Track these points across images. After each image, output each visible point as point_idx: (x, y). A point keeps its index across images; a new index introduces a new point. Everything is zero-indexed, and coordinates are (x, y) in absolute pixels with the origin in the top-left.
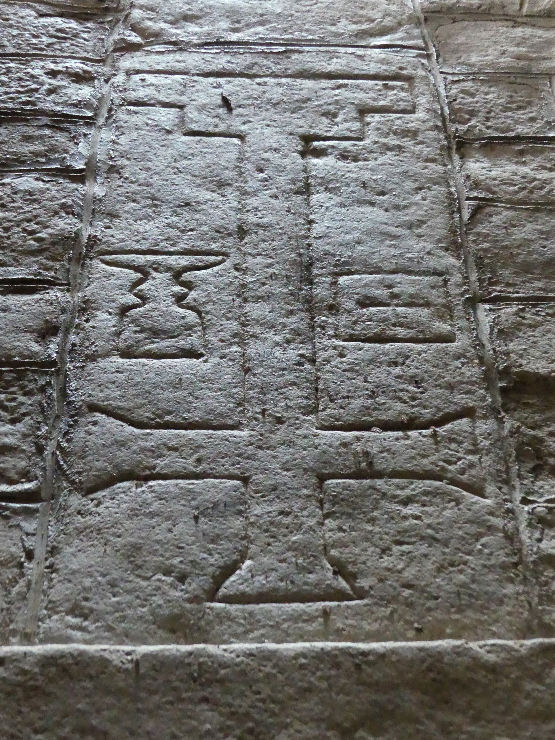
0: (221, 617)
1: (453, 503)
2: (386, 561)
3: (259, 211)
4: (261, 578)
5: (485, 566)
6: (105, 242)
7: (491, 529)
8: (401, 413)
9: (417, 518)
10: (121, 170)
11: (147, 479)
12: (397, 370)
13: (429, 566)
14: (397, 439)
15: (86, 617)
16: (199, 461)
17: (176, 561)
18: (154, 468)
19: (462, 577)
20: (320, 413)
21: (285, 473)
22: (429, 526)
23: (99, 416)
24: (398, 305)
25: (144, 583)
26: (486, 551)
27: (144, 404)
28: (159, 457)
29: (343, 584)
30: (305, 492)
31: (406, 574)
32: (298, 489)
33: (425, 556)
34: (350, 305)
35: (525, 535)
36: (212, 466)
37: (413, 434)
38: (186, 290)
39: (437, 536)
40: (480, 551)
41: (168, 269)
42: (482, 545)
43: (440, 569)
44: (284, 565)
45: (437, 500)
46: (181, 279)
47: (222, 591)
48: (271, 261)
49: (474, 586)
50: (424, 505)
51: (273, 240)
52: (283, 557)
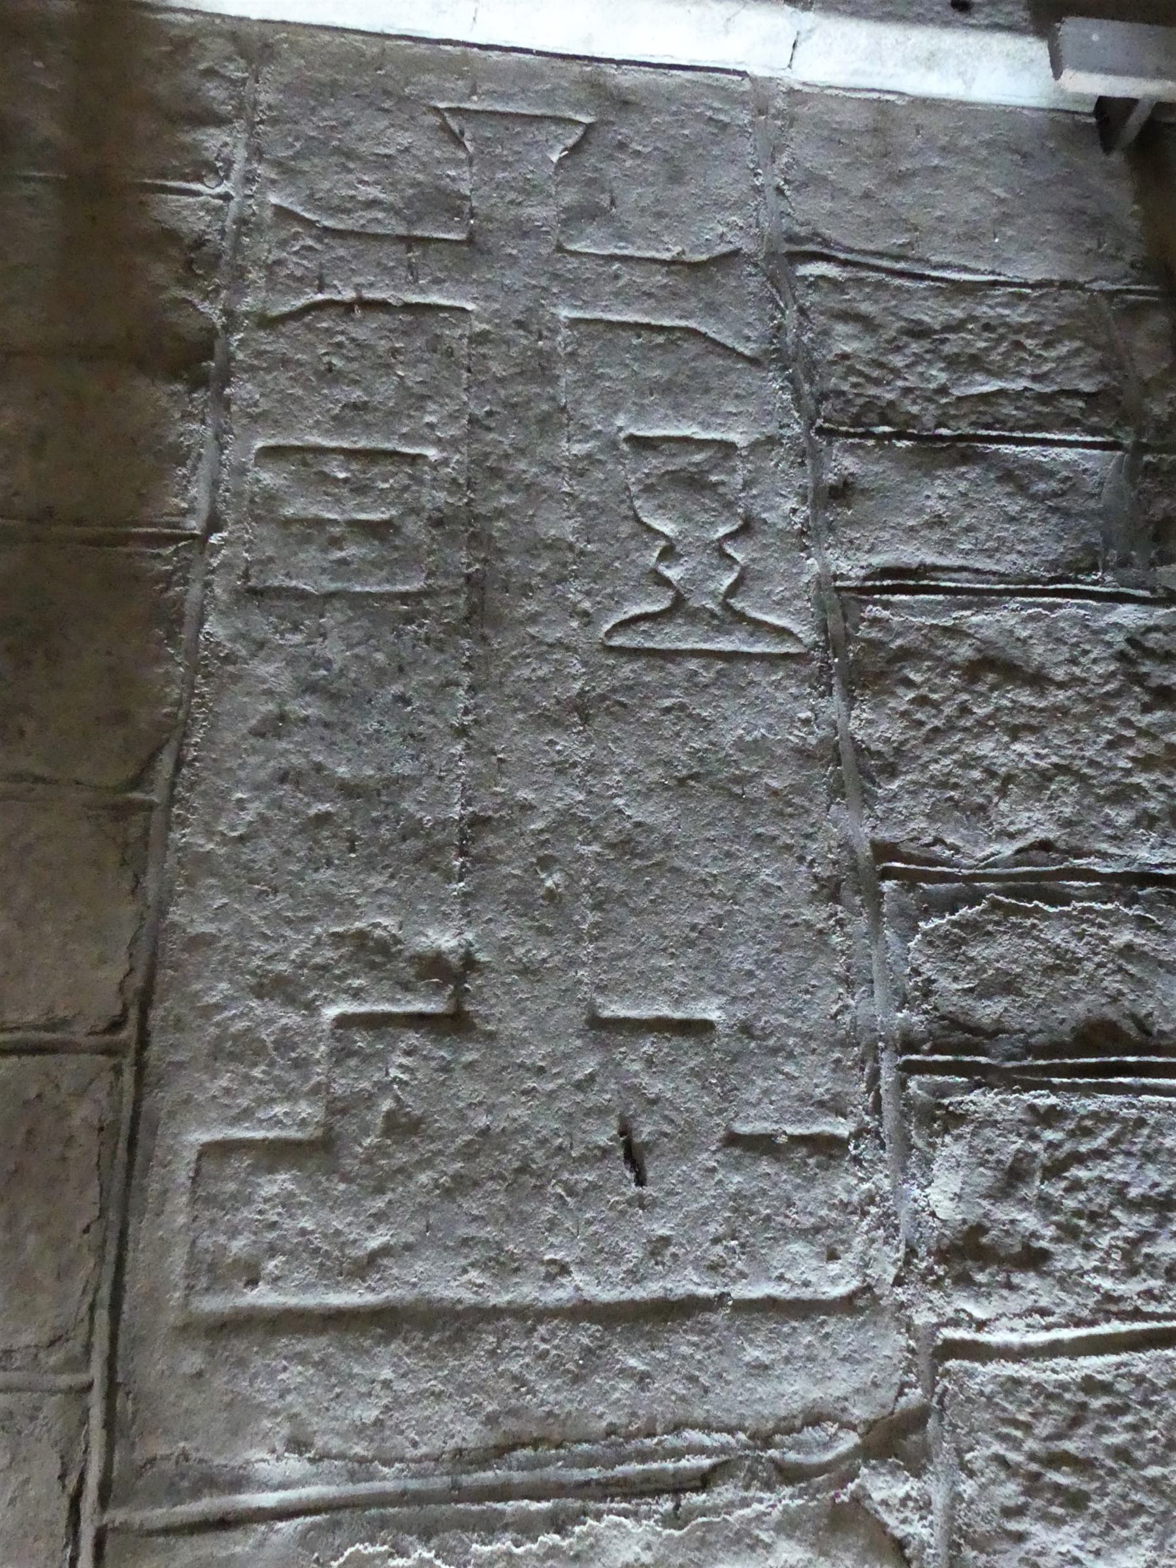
0: (579, 106)
1: (318, 196)
2: (405, 139)
3: (553, 764)
4: (539, 138)
5: (296, 123)
6: (803, 681)
7: (278, 164)
8: (360, 322)
9: (361, 182)
10: (815, 887)
11: (673, 262)
12: (357, 395)
13: (357, 128)
14: (371, 285)
15: (710, 119)
16: (617, 277)
17: (628, 163)
18: (668, 274)
19: (325, 114)
20: (467, 333)
21: (514, 252)
22: (350, 171)
23: (746, 349)
24: (334, 522)
25: (659, 145)
26: (290, 139)
27: (693, 360)
28: (665, 286)
29: (454, 124)
30: (490, 226)
31: (386, 123)
32: (500, 229)
33: (361, 139)
34: (412, 526)
35: (241, 154)
36: (600, 270)
37: (349, 295)
38: (661, 568)
39: (343, 160)
40: (297, 139)
41: (694, 616)
42: (293, 146)
43: (348, 124)
44: (516, 148)
45: (336, 202)
46: (671, 593)
47: (579, 131)
48: (532, 630)
49: (313, 103)
50: (353, 197)
51: (529, 680)
52: (516, 157)
